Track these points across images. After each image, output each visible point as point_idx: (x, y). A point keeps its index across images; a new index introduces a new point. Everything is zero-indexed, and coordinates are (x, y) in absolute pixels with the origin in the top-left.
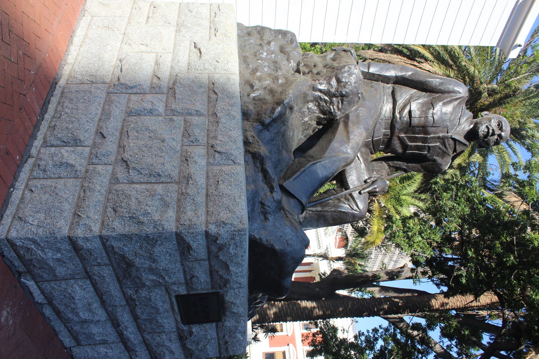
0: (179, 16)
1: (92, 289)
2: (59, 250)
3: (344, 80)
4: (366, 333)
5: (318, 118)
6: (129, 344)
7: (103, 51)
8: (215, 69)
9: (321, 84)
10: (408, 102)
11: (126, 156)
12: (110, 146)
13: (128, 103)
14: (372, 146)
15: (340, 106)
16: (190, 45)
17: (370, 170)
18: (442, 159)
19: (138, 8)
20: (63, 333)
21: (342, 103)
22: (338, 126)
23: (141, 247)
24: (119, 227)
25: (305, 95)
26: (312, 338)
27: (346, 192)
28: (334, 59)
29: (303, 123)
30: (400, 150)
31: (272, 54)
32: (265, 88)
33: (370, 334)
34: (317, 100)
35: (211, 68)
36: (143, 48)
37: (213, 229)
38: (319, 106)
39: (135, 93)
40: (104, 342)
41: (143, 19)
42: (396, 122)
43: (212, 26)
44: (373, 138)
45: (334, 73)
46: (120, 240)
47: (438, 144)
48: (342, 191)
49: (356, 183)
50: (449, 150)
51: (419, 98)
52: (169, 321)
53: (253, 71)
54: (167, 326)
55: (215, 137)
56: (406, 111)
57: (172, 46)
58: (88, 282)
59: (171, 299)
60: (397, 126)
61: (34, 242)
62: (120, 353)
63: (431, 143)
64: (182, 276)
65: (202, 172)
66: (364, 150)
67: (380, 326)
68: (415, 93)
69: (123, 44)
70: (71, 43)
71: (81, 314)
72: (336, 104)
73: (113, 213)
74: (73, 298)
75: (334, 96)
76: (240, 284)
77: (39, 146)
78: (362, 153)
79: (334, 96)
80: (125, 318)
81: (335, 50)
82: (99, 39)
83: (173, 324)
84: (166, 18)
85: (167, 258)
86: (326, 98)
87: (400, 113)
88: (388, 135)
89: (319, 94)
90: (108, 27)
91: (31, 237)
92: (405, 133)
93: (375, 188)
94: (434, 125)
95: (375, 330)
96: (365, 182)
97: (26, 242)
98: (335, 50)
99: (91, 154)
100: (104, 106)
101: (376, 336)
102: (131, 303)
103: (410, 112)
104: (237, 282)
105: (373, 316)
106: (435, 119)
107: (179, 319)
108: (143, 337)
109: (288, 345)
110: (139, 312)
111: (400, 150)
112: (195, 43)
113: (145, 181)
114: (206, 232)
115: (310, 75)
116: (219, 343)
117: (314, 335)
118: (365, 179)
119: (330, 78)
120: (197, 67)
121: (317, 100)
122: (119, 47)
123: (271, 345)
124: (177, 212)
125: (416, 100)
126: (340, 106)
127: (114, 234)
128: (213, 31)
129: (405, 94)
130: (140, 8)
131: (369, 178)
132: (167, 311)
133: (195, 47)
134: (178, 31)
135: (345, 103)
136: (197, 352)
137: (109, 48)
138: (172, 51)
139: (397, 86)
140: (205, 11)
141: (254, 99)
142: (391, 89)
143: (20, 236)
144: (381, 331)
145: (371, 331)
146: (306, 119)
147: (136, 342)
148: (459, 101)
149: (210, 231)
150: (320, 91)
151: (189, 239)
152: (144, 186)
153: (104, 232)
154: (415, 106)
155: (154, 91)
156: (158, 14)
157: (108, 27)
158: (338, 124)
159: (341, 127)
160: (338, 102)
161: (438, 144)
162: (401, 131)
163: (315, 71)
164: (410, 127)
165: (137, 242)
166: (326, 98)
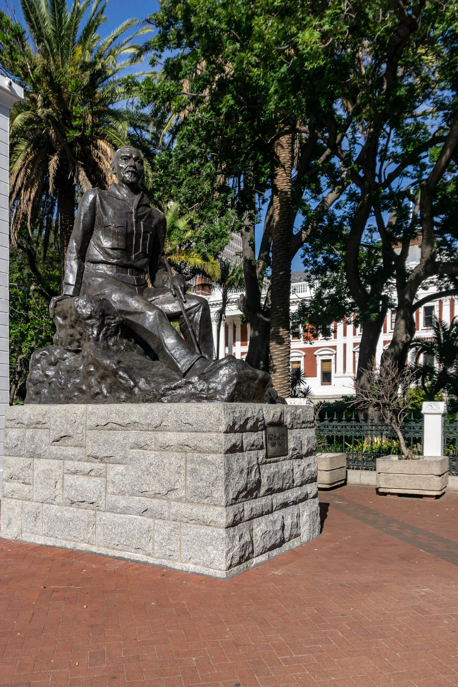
0: (21, 456)
1: (260, 518)
2: (234, 536)
3: (89, 313)
4: (308, 274)
5: (121, 337)
6: (301, 497)
7: (63, 519)
8: (82, 424)
9: (93, 333)
10: (103, 250)
11: (164, 491)
12: (155, 503)
13: (116, 494)
14: (142, 287)
15: (112, 317)
16: (55, 445)
17: (164, 291)
18: (154, 218)
19: (13, 493)
20: (291, 545)
21: (109, 315)
22: (130, 320)
23: (233, 479)
24: (219, 494)
25: (104, 348)
26: (309, 333)
27: (184, 315)
28: (65, 318)
29: (126, 351)
30: (146, 260)
31: (59, 374)
32: (99, 383)
33: (309, 269)
34: (106, 338)
35: (81, 428)
36: (59, 486)
37: (223, 428)
38: (111, 336)
39: (106, 489)
40: (298, 516)
41: (27, 488)
42: (121, 263)
43: (34, 426)
44: (135, 286)
45: (83, 321)
46: (228, 493)
47: (142, 223)
48: (184, 318)
49: (176, 304)
50: (146, 211)
51: (99, 238)
52: (285, 465)
53: (81, 392)
54: (288, 467)
55: (149, 424)
56: (111, 252)
57: (57, 461)
58: (255, 520)
59: (270, 462)
60: (125, 262)
61: (228, 553)
62: (307, 505)
63: (140, 230)
64: (253, 452)
65: (178, 435)
66: (145, 295)
67: (302, 257)
68: (93, 241)
69: (55, 503)
70: (54, 547)
71: (277, 529)
72: (109, 321)
73: (209, 498)
74: (266, 532)
75: (103, 322)
76: (260, 410)
77: (153, 559)
78: (148, 297)
79: (103, 322)
80: (279, 498)
81: (54, 316)
82: (49, 524)
83: (287, 462)
84: (25, 467)
85: (242, 460)
86: (104, 329)
87: (113, 259)
88: (133, 271)
89: (101, 335)
90: (36, 518)
91: (225, 554)
92: (132, 255)
93: (181, 288)
94: (125, 226)
95: (306, 263)
96: (175, 296)
97: (228, 558)
98: (54, 316)
99: (160, 518)
100: (117, 513)
101: (312, 262)
102: (271, 491)
103: (112, 249)
104: (259, 412)
105: (290, 271)
106: (119, 225)
107: (284, 457)
108: (296, 486)
109: (315, 356)
110: (276, 487)
111: (146, 260)
112: (54, 441)
113: (184, 477)
114: (226, 432)
115: (82, 342)
116: (304, 428)
117: (305, 331)
118: (172, 297)
119: (87, 324)
120: (80, 439)
121: (106, 338)
122: (57, 506)
123: (315, 376)
124: (209, 453)
125: (101, 242)
126: (112, 317)
127: (224, 497)
128: (39, 426)
129: (95, 252)
130: (13, 491)
131: (172, 292)
132: (277, 465)
133: (58, 441)
134: (39, 456)
135: (109, 313)
136: (310, 446)
137: (59, 514)
138: (62, 461)
139: (86, 258)
140: (14, 433)
141: (109, 392)
142: (89, 264)
143: (224, 562)
144: (307, 257)
145: (306, 268)
146: (122, 348)
147: (300, 492)
148: (103, 199)
149: (224, 430)
150: (98, 334)
151: (229, 445)
152: (188, 478)
153: (223, 503)
154: (107, 244)
155: (104, 474)
156: (21, 475)
157: (36, 518)
158: (127, 320)
159: (130, 318)
160: (108, 319)
161: (142, 223)
162: (129, 259)
163: (78, 337)
164: (126, 250)
165: (230, 482)
166: (104, 329)
